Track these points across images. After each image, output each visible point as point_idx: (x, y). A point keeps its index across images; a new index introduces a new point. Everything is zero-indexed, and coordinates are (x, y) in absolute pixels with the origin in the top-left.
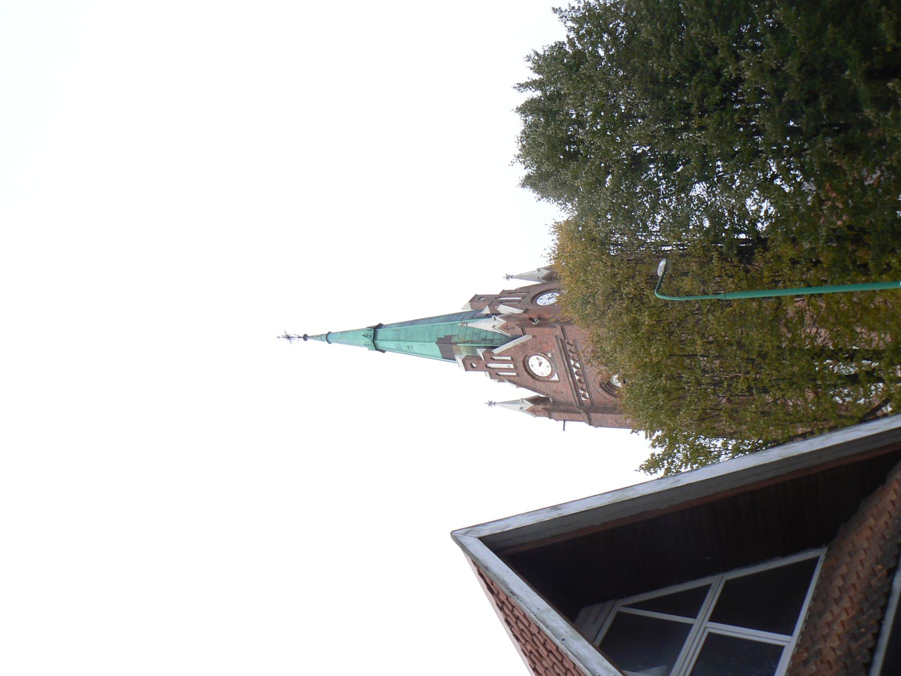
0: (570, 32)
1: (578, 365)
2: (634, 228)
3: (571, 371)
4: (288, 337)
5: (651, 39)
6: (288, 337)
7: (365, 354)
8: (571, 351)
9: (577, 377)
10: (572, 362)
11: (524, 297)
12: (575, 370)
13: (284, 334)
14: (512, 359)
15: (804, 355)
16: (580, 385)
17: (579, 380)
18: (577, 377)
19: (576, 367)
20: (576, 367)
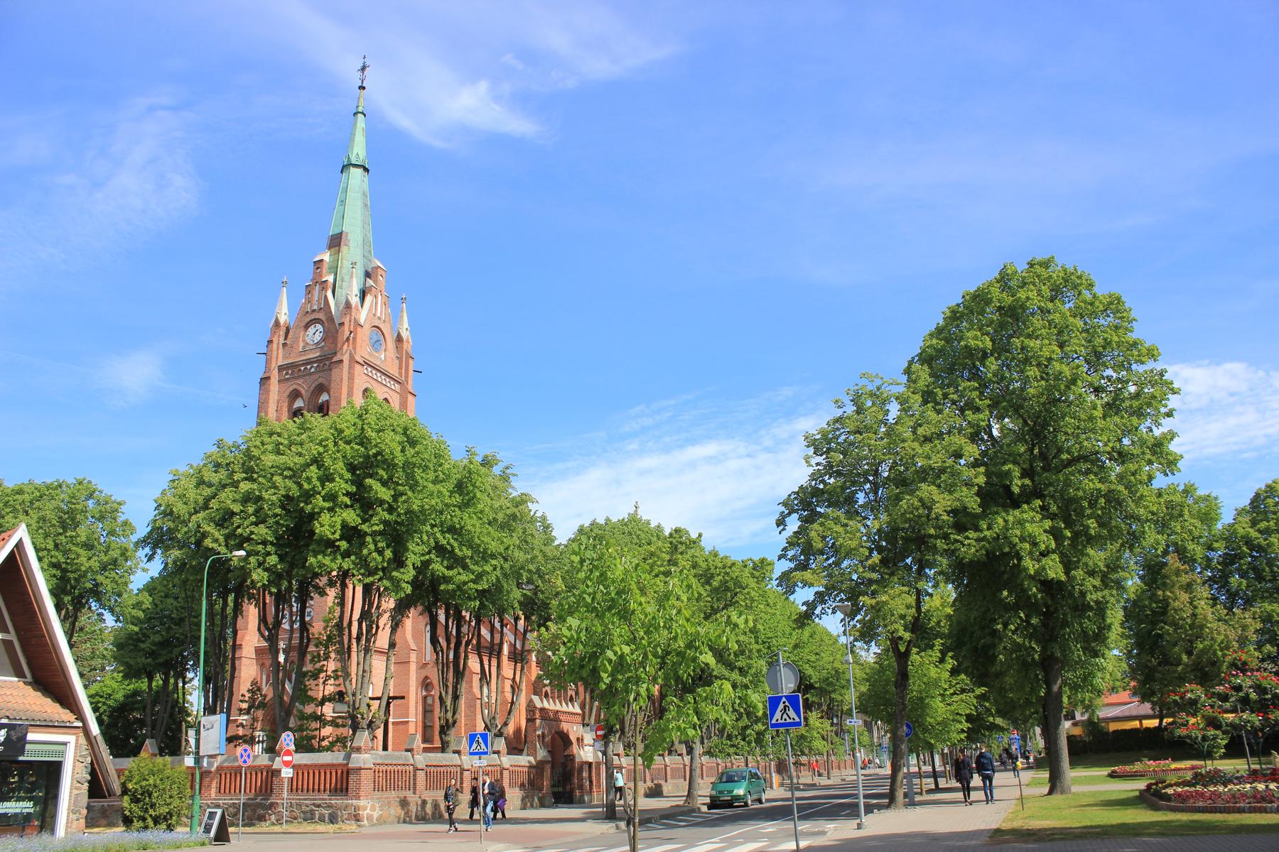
0: (954, 512)
1: (313, 370)
2: (140, 736)
3: (308, 364)
4: (363, 69)
5: (1226, 787)
6: (363, 69)
7: (261, 375)
8: (325, 364)
9: (302, 368)
10: (315, 365)
11: (379, 318)
12: (309, 367)
13: (367, 64)
14: (321, 309)
15: (962, 520)
16: (296, 370)
17: (300, 370)
18: (302, 368)
19: (311, 368)
20: (311, 368)
